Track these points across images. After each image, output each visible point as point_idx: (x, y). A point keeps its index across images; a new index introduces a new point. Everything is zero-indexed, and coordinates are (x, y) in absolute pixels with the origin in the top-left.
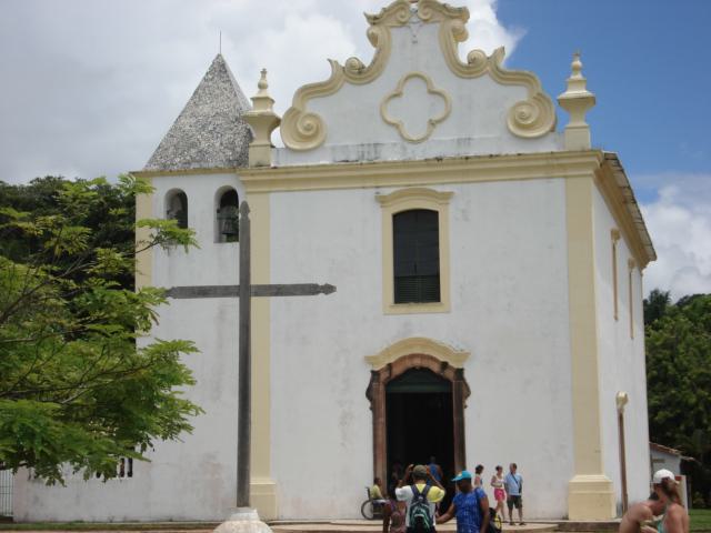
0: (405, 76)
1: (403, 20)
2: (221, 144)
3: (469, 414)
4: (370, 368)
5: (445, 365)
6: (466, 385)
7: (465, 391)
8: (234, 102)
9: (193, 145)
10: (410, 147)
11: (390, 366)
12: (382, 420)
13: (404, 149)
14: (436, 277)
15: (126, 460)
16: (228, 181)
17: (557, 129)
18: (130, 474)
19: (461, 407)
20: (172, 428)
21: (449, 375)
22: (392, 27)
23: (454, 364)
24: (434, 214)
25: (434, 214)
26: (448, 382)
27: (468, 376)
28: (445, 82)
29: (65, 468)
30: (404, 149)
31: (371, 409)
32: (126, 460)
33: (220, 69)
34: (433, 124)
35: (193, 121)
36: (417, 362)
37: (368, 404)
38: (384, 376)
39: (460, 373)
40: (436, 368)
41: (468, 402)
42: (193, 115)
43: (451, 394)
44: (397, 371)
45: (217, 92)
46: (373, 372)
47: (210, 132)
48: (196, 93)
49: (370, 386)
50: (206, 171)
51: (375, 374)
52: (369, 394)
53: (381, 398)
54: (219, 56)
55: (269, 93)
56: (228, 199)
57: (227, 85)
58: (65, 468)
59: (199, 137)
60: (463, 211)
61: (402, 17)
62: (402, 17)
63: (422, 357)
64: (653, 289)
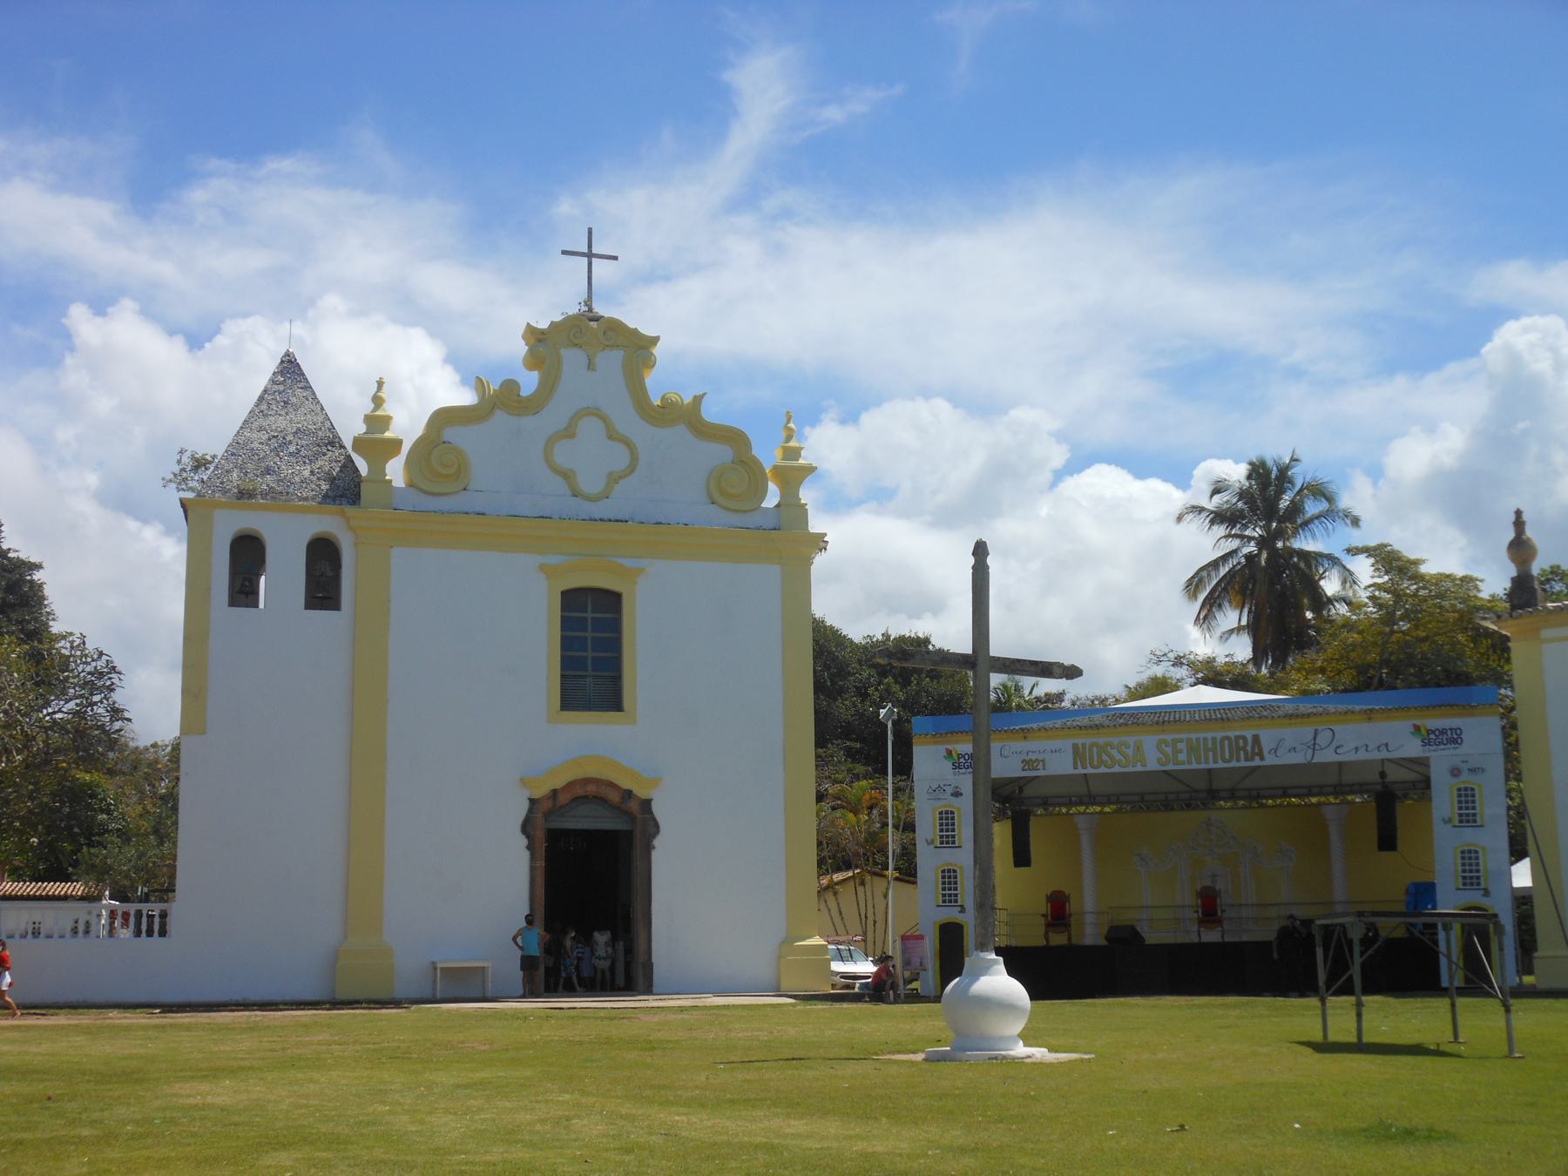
2: (312, 472)
3: (656, 856)
4: (526, 794)
6: (654, 820)
12: (541, 864)
16: (327, 523)
18: (163, 933)
19: (649, 848)
21: (633, 806)
23: (641, 793)
27: (657, 809)
29: (657, 402)
33: (290, 369)
37: (524, 841)
39: (646, 804)
40: (614, 797)
41: (656, 842)
46: (531, 800)
47: (291, 454)
48: (261, 399)
51: (532, 801)
52: (526, 827)
53: (540, 834)
54: (288, 354)
55: (69, 925)
56: (323, 555)
58: (657, 402)
64: (1515, 510)
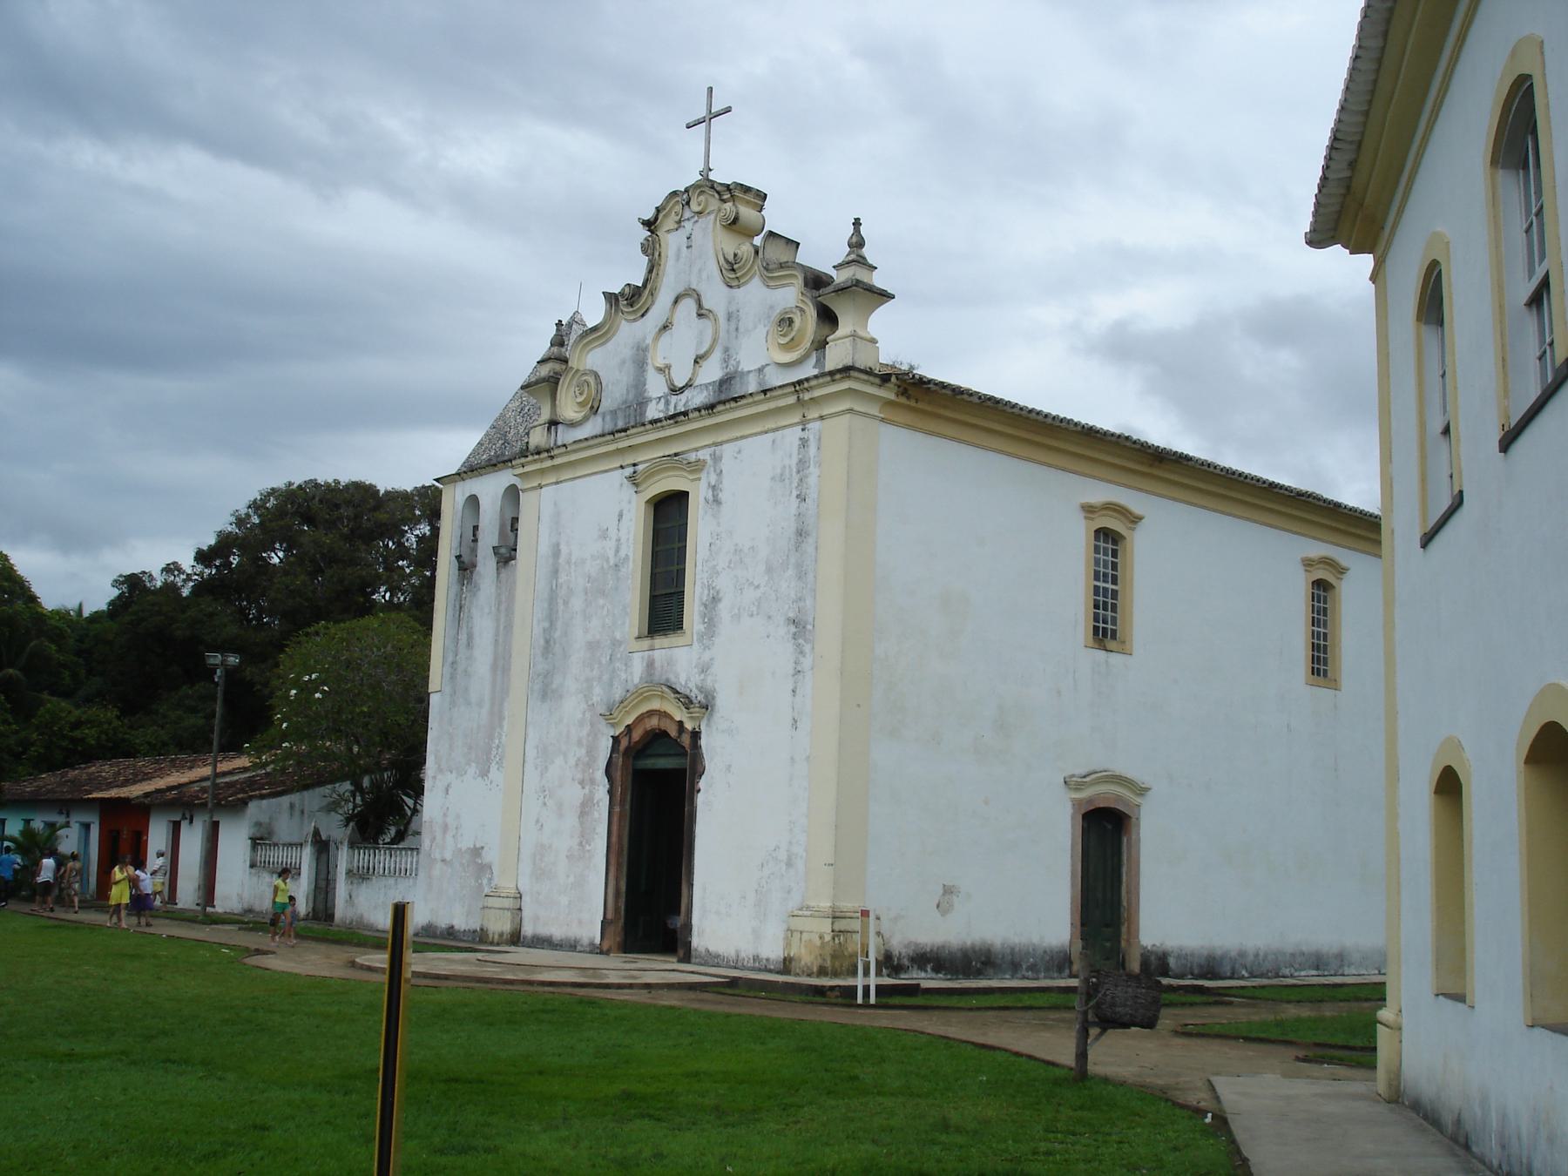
19: (695, 790)
21: (686, 740)
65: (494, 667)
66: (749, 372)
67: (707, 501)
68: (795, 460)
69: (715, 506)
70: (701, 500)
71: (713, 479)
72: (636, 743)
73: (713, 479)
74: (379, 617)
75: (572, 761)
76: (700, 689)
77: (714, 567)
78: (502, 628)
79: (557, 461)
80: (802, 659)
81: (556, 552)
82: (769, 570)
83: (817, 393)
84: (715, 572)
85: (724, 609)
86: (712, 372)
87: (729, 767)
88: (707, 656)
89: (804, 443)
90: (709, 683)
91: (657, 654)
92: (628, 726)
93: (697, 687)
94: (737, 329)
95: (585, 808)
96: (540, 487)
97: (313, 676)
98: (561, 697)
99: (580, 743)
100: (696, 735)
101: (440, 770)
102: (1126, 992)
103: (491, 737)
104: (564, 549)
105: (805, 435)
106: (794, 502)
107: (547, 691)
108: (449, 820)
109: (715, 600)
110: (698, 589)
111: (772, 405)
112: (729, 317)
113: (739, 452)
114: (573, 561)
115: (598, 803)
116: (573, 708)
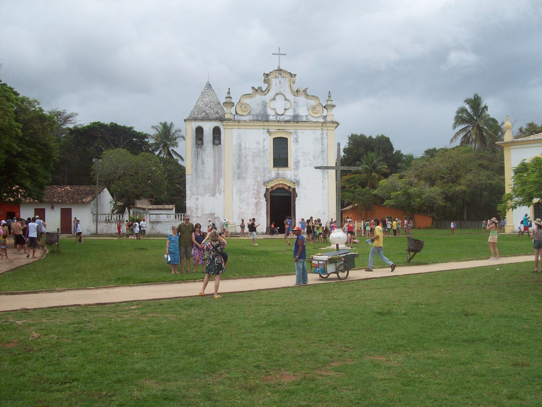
0: (450, 141)
1: (276, 76)
5: (290, 187)
7: (296, 196)
8: (216, 97)
9: (204, 111)
10: (279, 117)
11: (272, 187)
13: (276, 117)
14: (287, 159)
15: (177, 215)
17: (286, 101)
19: (294, 200)
20: (112, 123)
21: (291, 190)
22: (272, 78)
24: (287, 139)
25: (287, 139)
26: (290, 193)
28: (289, 96)
30: (276, 117)
31: (266, 200)
32: (177, 215)
34: (285, 109)
35: (202, 103)
36: (281, 186)
38: (270, 190)
40: (287, 188)
42: (202, 101)
43: (291, 197)
44: (274, 189)
45: (209, 94)
46: (266, 189)
47: (209, 107)
49: (266, 193)
50: (211, 120)
51: (267, 189)
52: (265, 196)
56: (217, 132)
57: (213, 92)
59: (206, 109)
60: (296, 139)
61: (276, 75)
62: (276, 75)
63: (282, 184)
65: (215, 170)
66: (303, 116)
67: (294, 141)
68: (320, 137)
69: (297, 142)
70: (292, 141)
71: (295, 137)
72: (274, 190)
73: (295, 137)
74: (25, 168)
75: (251, 193)
76: (295, 180)
77: (297, 155)
78: (217, 161)
79: (240, 124)
80: (324, 176)
81: (240, 145)
82: (314, 158)
83: (328, 125)
84: (297, 156)
85: (301, 164)
86: (290, 113)
87: (305, 196)
88: (296, 173)
89: (322, 134)
90: (297, 179)
91: (280, 172)
92: (272, 187)
93: (294, 179)
94: (297, 106)
95: (257, 204)
96: (232, 129)
97: (475, 117)
98: (245, 179)
99: (254, 189)
100: (294, 189)
101: (193, 194)
102: (403, 259)
103: (215, 187)
104: (243, 145)
105: (322, 132)
106: (320, 146)
107: (240, 176)
108: (199, 207)
109: (298, 162)
110: (292, 159)
111: (315, 125)
112: (295, 102)
113: (303, 132)
114: (247, 148)
115: (262, 203)
116: (250, 181)
